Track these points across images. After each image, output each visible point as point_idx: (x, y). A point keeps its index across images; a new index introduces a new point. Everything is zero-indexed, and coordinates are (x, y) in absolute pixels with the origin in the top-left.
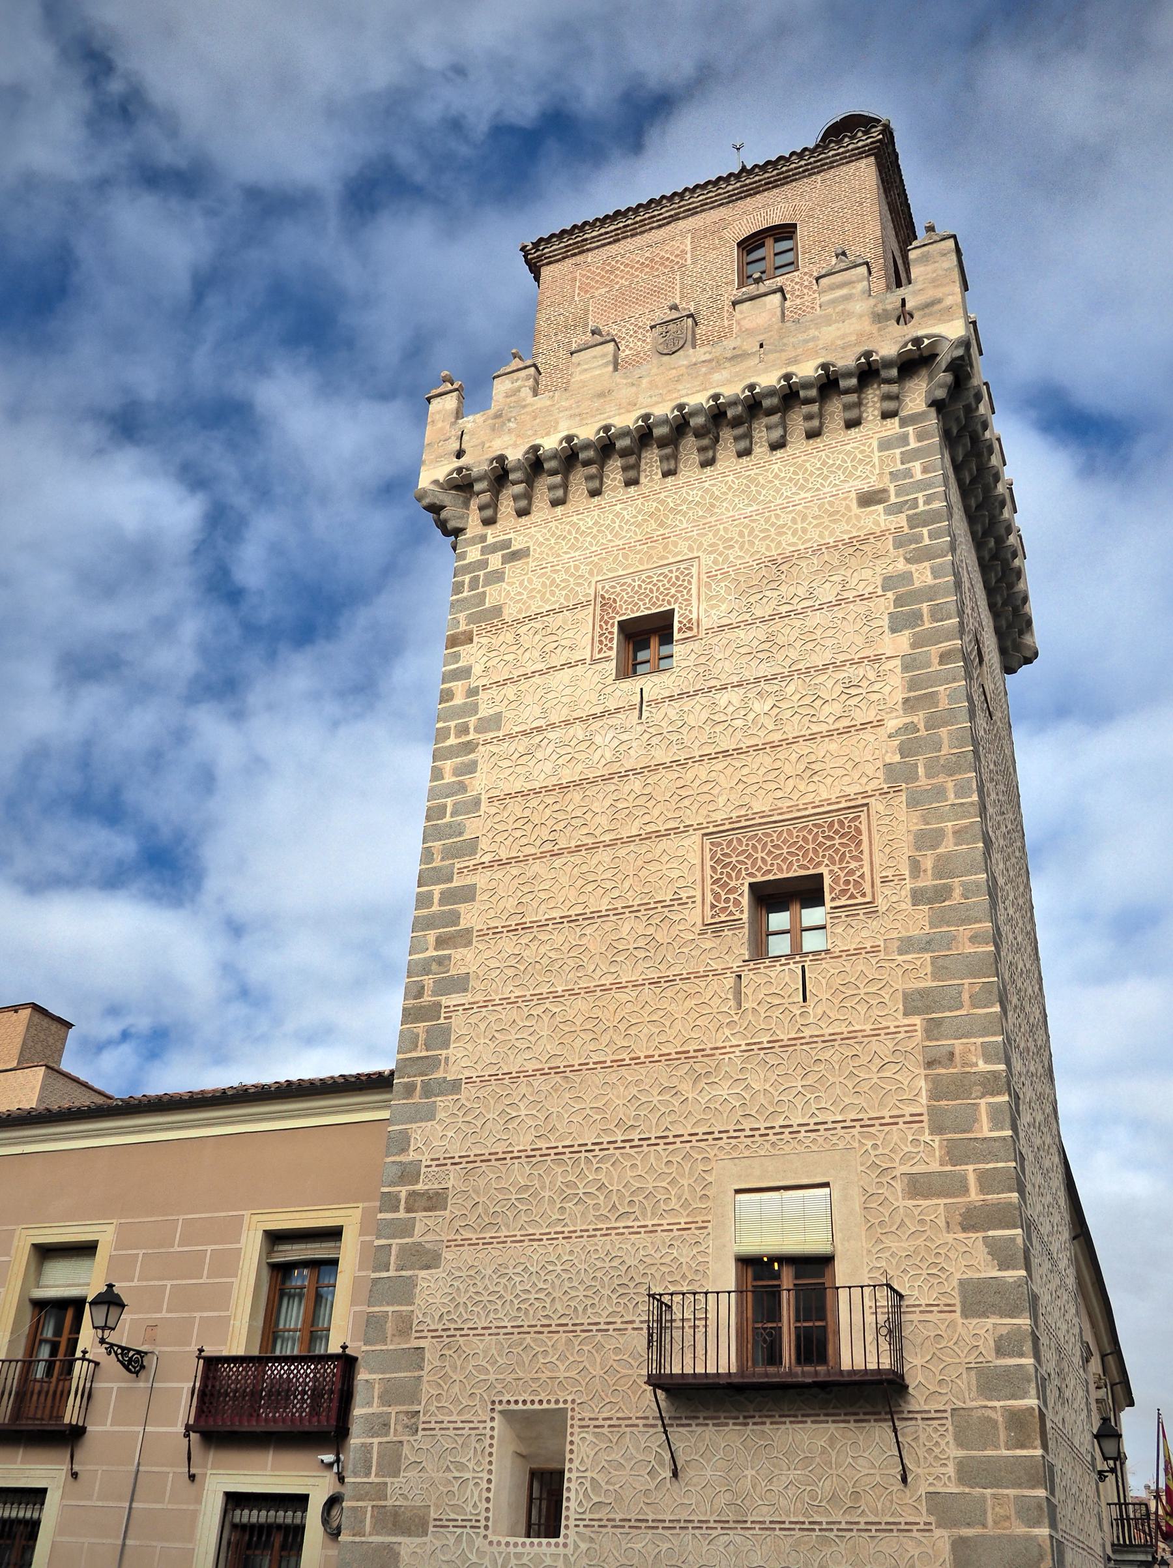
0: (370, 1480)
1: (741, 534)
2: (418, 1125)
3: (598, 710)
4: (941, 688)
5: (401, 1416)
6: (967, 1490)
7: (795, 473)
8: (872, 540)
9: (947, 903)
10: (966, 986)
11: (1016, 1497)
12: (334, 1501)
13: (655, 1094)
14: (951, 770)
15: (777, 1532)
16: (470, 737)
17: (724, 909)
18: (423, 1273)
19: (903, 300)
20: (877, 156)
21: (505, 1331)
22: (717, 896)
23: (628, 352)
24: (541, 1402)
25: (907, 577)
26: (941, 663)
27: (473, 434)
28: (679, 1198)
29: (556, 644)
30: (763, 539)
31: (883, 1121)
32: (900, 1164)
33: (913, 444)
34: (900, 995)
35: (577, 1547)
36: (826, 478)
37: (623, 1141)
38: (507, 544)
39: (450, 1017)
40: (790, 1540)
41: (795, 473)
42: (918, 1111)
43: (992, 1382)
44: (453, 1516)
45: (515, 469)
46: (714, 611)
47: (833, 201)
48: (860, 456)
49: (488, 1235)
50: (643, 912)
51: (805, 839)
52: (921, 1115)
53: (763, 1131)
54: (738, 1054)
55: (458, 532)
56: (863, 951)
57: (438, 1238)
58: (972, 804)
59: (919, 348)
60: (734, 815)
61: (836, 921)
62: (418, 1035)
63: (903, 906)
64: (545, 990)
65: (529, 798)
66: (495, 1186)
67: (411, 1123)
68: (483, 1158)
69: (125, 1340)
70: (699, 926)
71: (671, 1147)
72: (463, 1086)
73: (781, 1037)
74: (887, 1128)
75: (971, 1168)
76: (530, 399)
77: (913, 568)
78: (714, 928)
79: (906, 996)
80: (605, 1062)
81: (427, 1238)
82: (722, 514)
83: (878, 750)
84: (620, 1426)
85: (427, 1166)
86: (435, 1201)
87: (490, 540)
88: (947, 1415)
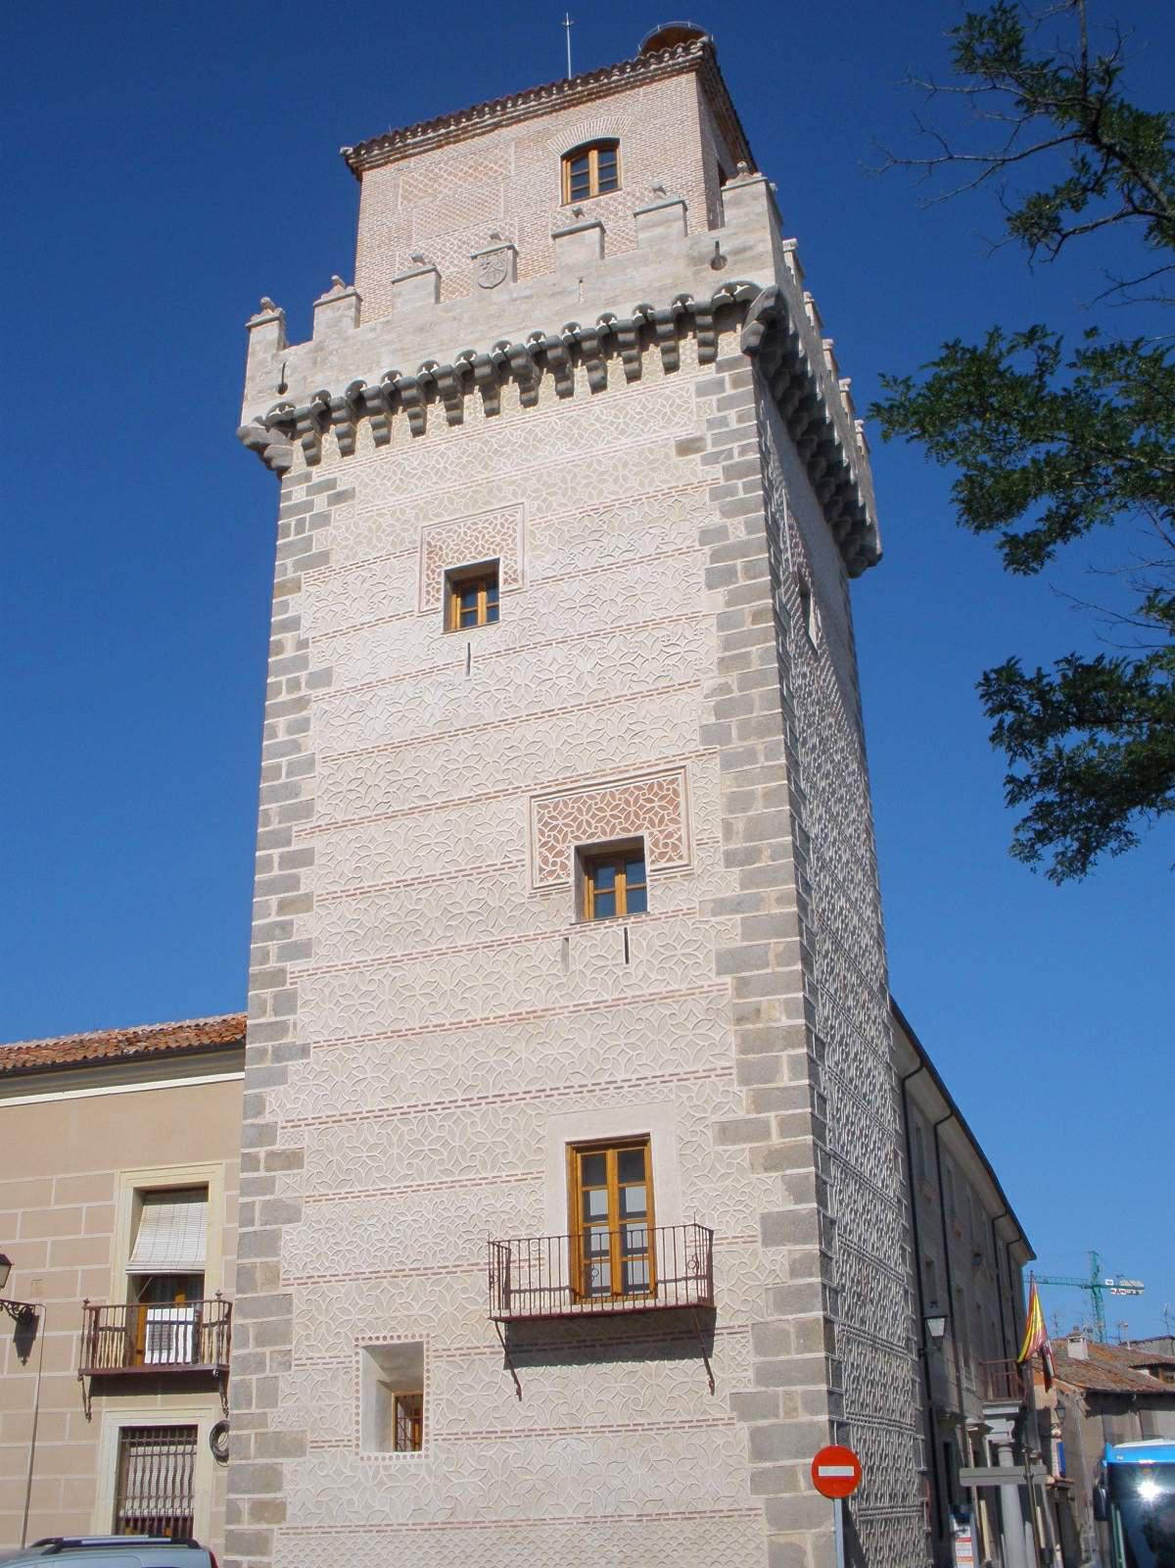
0: (252, 1411)
1: (564, 480)
2: (272, 1088)
3: (426, 666)
4: (753, 649)
5: (275, 1355)
6: (763, 1389)
7: (616, 417)
8: (690, 491)
9: (756, 865)
10: (772, 946)
11: (804, 1393)
12: (220, 1429)
13: (492, 1054)
14: (762, 730)
15: (607, 1434)
16: (302, 693)
17: (551, 873)
18: (286, 1227)
19: (717, 244)
20: (697, 71)
21: (363, 1276)
22: (545, 861)
23: (452, 269)
24: (399, 1337)
25: (721, 532)
26: (754, 622)
27: (295, 370)
28: (516, 1152)
29: (383, 594)
30: (587, 485)
31: (697, 1075)
32: (713, 1113)
33: (729, 391)
34: (713, 955)
35: (436, 1457)
36: (645, 423)
37: (463, 1100)
38: (330, 484)
39: (296, 983)
40: (617, 1440)
41: (616, 417)
42: (727, 1064)
43: (786, 1299)
44: (328, 1438)
45: (339, 408)
46: (539, 562)
47: (656, 116)
48: (678, 401)
49: (343, 1191)
50: (475, 876)
51: (627, 802)
52: (730, 1068)
53: (590, 1088)
54: (567, 1015)
55: (283, 470)
56: (680, 913)
57: (297, 1195)
58: (780, 766)
59: (732, 295)
60: (560, 777)
61: (656, 884)
62: (265, 1001)
63: (717, 869)
64: (385, 955)
65: (362, 757)
66: (346, 1145)
67: (265, 1086)
68: (334, 1119)
69: (13, 1294)
70: (528, 891)
71: (508, 1104)
72: (312, 1050)
73: (606, 997)
74: (700, 1081)
75: (772, 1114)
76: (351, 331)
77: (728, 522)
78: (544, 892)
79: (719, 956)
80: (444, 1025)
81: (289, 1194)
82: (546, 457)
83: (692, 710)
84: (469, 1354)
85: (283, 1128)
86: (292, 1160)
87: (315, 479)
88: (749, 1329)
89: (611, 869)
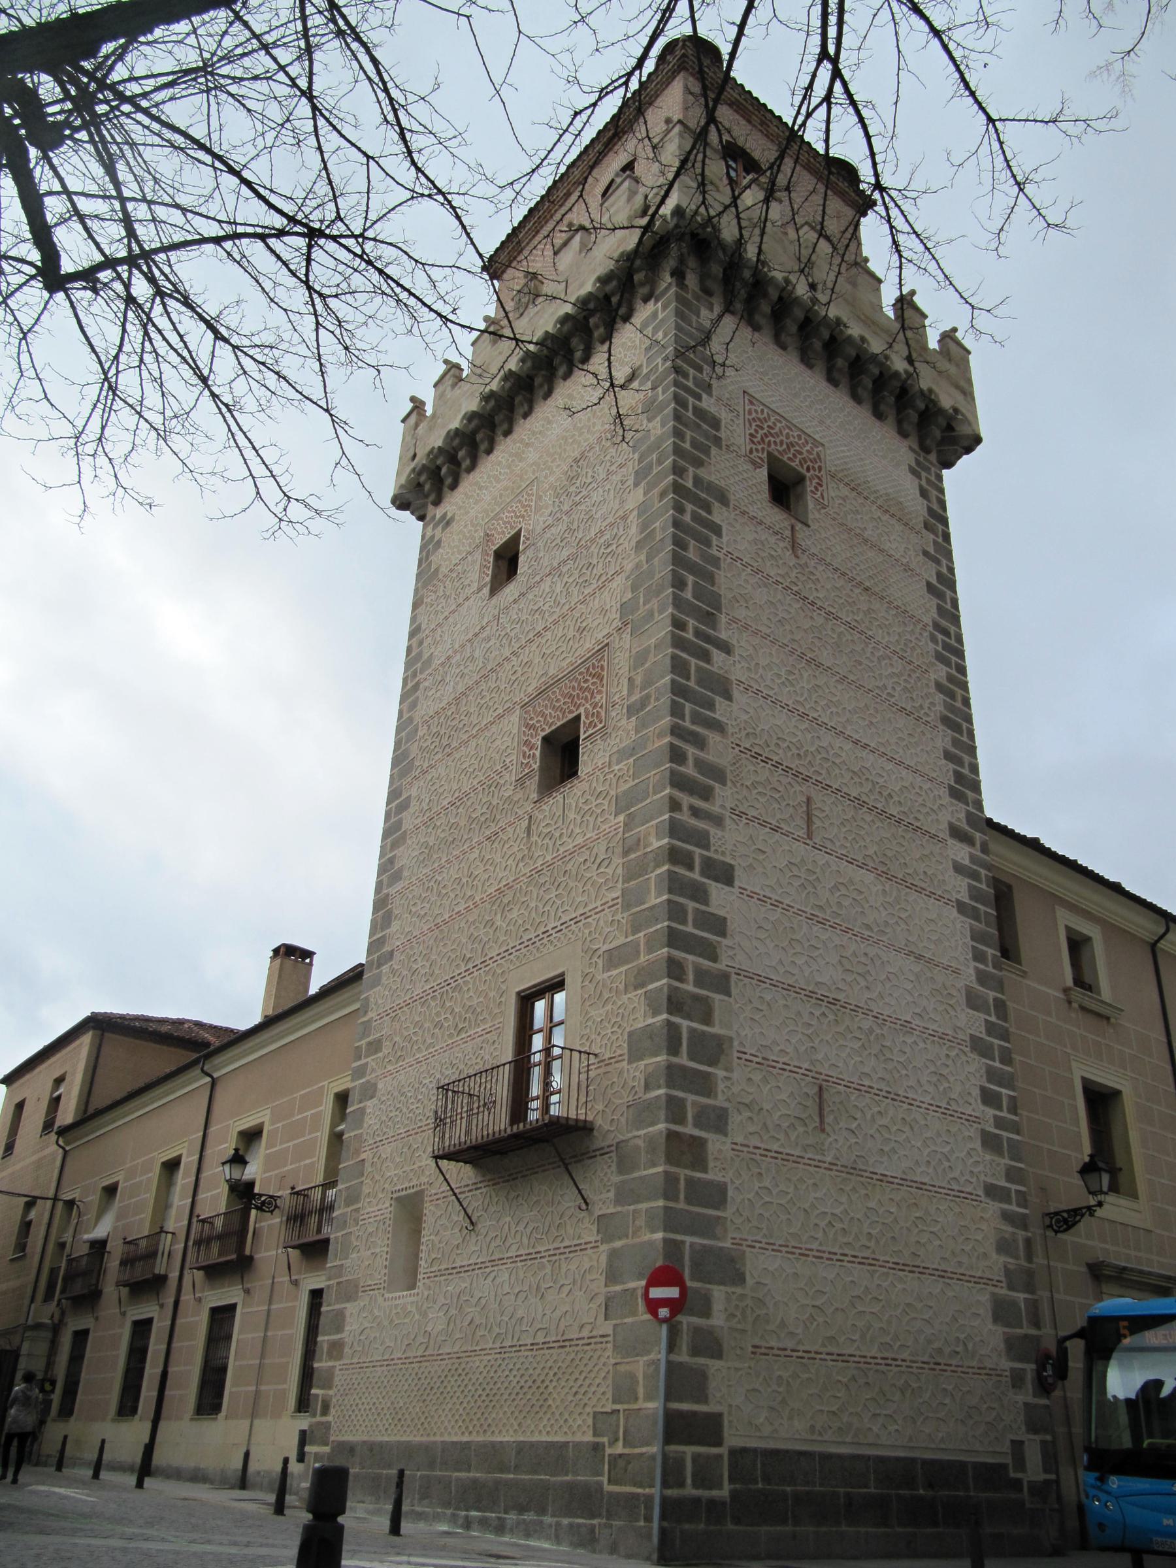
89: (562, 755)
